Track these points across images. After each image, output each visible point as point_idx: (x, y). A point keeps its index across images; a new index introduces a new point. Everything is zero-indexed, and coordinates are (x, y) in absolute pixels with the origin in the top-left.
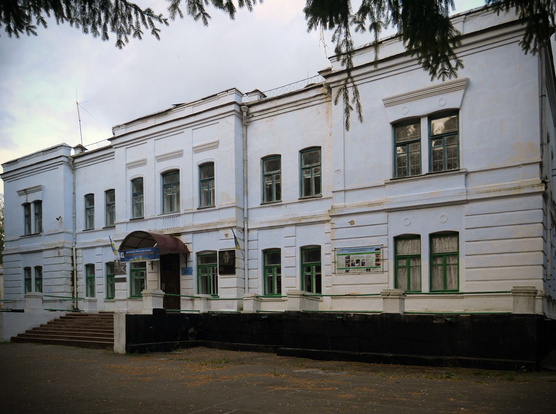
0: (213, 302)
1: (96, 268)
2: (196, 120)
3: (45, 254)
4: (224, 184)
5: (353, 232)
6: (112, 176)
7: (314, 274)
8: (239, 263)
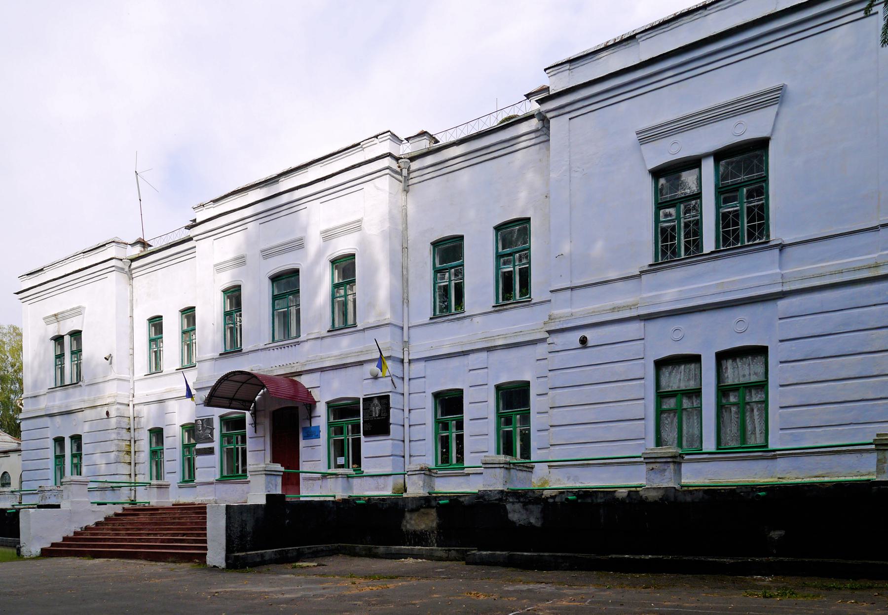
0: (356, 482)
8: (395, 416)
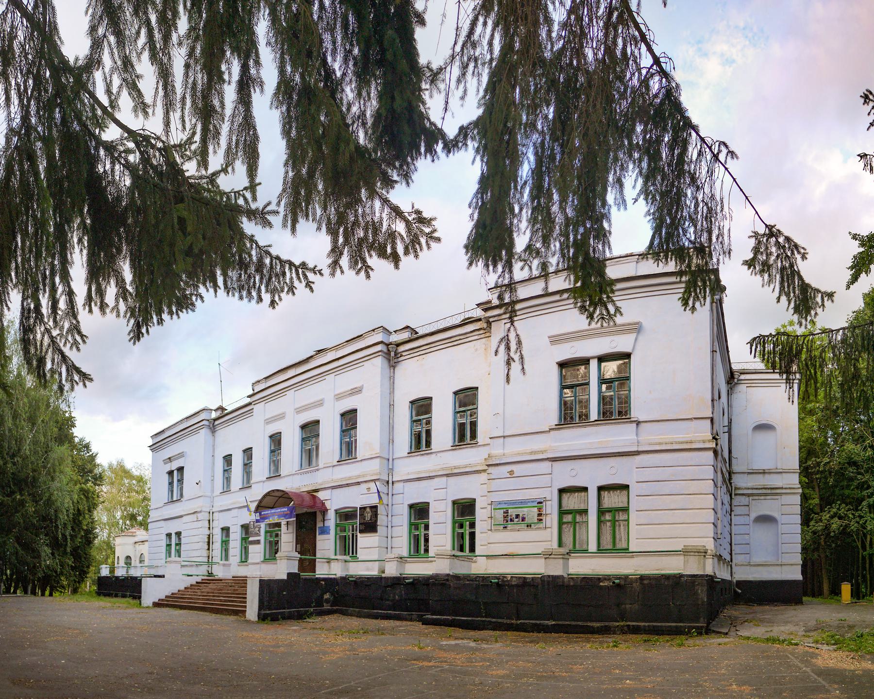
1: (231, 531)
2: (339, 365)
3: (185, 519)
4: (368, 434)
5: (512, 483)
6: (252, 434)
7: (467, 531)
8: (381, 520)
